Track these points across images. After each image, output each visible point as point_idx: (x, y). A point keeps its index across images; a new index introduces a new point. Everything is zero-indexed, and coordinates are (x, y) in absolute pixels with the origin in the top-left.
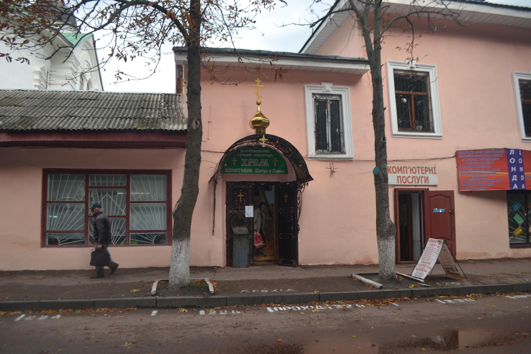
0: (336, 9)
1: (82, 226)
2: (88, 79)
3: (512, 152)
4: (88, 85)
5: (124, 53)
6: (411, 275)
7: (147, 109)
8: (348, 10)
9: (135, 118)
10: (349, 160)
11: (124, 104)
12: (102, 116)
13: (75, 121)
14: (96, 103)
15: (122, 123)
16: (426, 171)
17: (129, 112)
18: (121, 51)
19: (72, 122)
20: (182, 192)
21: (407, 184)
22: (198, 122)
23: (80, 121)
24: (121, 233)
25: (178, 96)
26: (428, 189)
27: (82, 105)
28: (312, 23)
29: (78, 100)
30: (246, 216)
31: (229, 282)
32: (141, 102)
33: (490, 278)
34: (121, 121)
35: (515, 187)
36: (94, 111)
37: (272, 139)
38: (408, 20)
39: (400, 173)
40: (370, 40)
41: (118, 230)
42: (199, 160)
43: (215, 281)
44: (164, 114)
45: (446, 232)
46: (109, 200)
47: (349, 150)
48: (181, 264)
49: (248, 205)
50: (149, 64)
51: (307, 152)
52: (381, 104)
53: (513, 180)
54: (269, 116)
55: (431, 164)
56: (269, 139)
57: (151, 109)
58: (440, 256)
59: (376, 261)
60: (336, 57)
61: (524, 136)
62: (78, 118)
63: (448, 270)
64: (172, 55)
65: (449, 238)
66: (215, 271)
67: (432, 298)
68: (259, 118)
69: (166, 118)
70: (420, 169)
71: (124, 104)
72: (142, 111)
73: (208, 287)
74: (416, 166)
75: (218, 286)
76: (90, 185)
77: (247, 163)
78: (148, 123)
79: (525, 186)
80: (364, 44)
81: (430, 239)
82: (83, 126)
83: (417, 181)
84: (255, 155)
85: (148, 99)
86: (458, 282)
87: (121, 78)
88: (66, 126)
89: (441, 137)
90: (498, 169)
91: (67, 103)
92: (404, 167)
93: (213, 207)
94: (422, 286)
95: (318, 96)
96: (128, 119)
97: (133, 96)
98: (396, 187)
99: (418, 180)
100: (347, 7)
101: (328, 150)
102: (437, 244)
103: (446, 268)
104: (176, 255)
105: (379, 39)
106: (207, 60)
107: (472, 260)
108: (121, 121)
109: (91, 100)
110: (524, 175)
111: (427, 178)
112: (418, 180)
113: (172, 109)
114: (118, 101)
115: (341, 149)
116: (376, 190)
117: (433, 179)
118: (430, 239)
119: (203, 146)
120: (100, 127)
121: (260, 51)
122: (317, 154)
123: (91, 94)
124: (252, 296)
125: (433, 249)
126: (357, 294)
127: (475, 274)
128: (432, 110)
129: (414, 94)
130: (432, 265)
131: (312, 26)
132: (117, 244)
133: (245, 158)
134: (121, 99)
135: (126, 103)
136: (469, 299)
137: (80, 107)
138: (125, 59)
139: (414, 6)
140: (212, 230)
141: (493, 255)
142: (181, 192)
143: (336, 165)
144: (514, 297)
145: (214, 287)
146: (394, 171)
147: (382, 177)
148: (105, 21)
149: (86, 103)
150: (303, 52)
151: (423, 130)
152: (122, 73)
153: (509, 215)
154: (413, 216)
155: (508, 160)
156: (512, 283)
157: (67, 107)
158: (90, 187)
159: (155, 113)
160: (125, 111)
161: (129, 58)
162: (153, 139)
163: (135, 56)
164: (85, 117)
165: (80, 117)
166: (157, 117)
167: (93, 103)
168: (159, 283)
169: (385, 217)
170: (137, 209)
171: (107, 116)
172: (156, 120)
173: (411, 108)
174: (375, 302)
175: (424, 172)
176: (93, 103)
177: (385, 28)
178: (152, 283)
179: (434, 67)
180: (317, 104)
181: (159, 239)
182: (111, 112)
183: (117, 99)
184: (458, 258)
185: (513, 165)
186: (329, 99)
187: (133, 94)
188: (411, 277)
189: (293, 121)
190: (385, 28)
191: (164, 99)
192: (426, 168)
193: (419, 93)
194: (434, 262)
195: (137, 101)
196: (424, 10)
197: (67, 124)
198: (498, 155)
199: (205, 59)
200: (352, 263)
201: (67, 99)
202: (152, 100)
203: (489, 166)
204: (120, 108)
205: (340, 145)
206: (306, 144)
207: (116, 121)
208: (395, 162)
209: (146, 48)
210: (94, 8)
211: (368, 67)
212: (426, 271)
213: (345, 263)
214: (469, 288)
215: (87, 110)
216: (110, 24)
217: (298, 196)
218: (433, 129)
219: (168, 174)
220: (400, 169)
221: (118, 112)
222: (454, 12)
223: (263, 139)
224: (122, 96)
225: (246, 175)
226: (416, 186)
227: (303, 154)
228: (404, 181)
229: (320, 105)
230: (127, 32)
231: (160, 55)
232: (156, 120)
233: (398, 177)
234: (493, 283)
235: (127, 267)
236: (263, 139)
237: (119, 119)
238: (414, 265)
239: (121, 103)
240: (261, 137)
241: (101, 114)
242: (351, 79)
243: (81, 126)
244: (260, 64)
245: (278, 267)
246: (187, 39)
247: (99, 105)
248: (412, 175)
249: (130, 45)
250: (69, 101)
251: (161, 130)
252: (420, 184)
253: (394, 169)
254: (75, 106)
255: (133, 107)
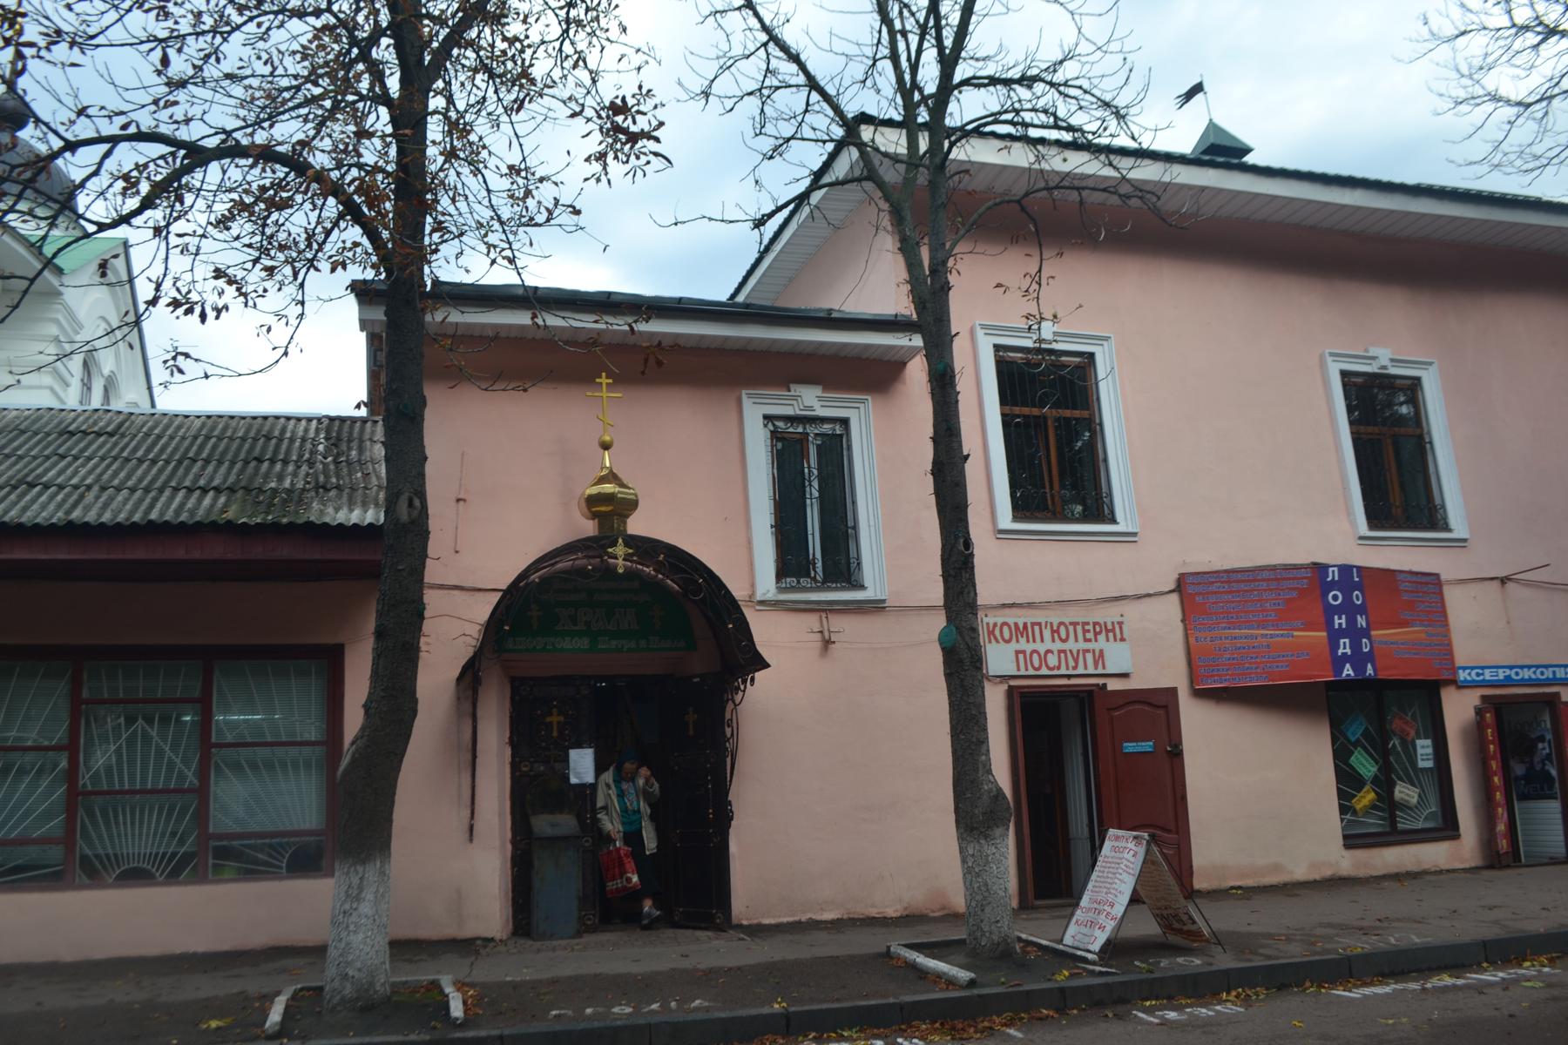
0: (826, 179)
1: (55, 825)
2: (106, 372)
3: (1333, 575)
4: (106, 389)
5: (194, 297)
6: (1060, 941)
7: (273, 461)
8: (859, 180)
9: (232, 490)
10: (875, 607)
11: (201, 447)
12: (130, 483)
13: (44, 498)
14: (115, 444)
15: (190, 505)
16: (1096, 634)
17: (215, 471)
18: (184, 291)
19: (33, 501)
20: (366, 713)
21: (1044, 671)
22: (417, 503)
23: (60, 497)
24: (182, 842)
25: (369, 424)
27: (70, 449)
28: (758, 216)
29: (61, 434)
30: (574, 780)
31: (515, 986)
32: (257, 440)
33: (1289, 939)
34: (187, 498)
35: (1348, 671)
36: (108, 467)
37: (646, 548)
38: (1023, 209)
39: (1023, 640)
40: (921, 264)
41: (173, 834)
42: (416, 614)
43: (472, 985)
44: (322, 478)
45: (1162, 813)
46: (147, 739)
47: (876, 579)
48: (361, 936)
49: (579, 746)
50: (269, 330)
51: (753, 585)
52: (955, 445)
53: (1340, 651)
54: (637, 483)
55: (1108, 615)
56: (637, 548)
57: (285, 462)
58: (1140, 878)
59: (959, 902)
60: (830, 311)
61: (1363, 527)
62: (53, 489)
63: (1169, 920)
64: (351, 305)
65: (1168, 827)
66: (477, 953)
67: (1120, 1009)
68: (608, 488)
69: (327, 490)
70: (1079, 628)
71: (201, 447)
72: (257, 469)
73: (447, 1003)
74: (1067, 621)
75: (479, 999)
76: (85, 694)
78: (271, 505)
79: (1375, 669)
80: (904, 275)
81: (1112, 832)
82: (68, 512)
83: (1071, 663)
85: (276, 433)
86: (1197, 956)
87: (181, 371)
88: (13, 513)
89: (1135, 534)
90: (1298, 623)
91: (25, 443)
92: (1033, 624)
93: (469, 756)
94: (1092, 973)
95: (780, 424)
96: (211, 493)
97: (233, 423)
98: (1013, 683)
99: (1076, 661)
100: (857, 173)
101: (814, 579)
102: (1131, 845)
103: (1162, 917)
104: (347, 907)
105: (944, 262)
106: (439, 317)
107: (1240, 888)
108: (187, 498)
109: (99, 434)
110: (1369, 638)
111: (1101, 652)
112: (1076, 661)
113: (349, 463)
114: (183, 438)
115: (850, 574)
116: (950, 694)
117: (1118, 657)
118: (1112, 832)
119: (432, 572)
120: (121, 517)
121: (610, 294)
122: (781, 590)
123: (100, 419)
124: (582, 1026)
125: (1120, 862)
126: (902, 1007)
127: (1245, 929)
128: (1106, 460)
129: (1053, 417)
130: (1119, 910)
131: (759, 223)
132: (119, 878)
134: (193, 432)
135: (209, 446)
136: (1229, 1005)
137: (63, 457)
138: (203, 317)
139: (1042, 171)
140: (466, 827)
141: (1300, 872)
142: (362, 712)
143: (838, 623)
144: (1356, 994)
145: (465, 1003)
146: (1007, 636)
147: (965, 655)
148: (133, 203)
149: (82, 445)
150: (740, 298)
151: (1086, 518)
152: (187, 355)
153: (1334, 752)
154: (1072, 763)
155: (1325, 595)
156: (1348, 952)
157: (21, 458)
158: (87, 702)
159: (295, 475)
160: (203, 468)
161: (211, 314)
162: (286, 551)
163: (226, 307)
164: (76, 487)
165: (61, 487)
166: (300, 485)
167: (104, 443)
168: (294, 997)
169: (976, 771)
170: (237, 767)
171: (145, 483)
172: (295, 496)
173: (1048, 456)
174: (953, 1028)
175: (1090, 635)
176: (104, 443)
177: (962, 232)
178: (268, 999)
179: (1107, 339)
180: (780, 445)
181: (305, 859)
182: (161, 471)
183: (181, 433)
184: (1199, 883)
185: (1339, 610)
186: (812, 430)
187: (232, 417)
188: (1061, 947)
189: (706, 493)
190: (962, 232)
191: (328, 431)
192: (1095, 624)
193: (1067, 413)
194: (1124, 899)
195: (243, 439)
196: (1065, 183)
197: (19, 507)
198: (1295, 584)
199: (437, 317)
200: (892, 912)
201: (23, 432)
202: (288, 435)
203: (1272, 616)
204: (186, 460)
205: (849, 564)
206: (746, 561)
207: (172, 498)
208: (1007, 611)
209: (268, 285)
210: (100, 164)
211: (917, 341)
212: (1102, 928)
213: (873, 912)
214: (1227, 972)
215: (83, 465)
216: (148, 213)
217: (728, 716)
218: (1112, 512)
219: (332, 660)
220: (1022, 631)
221: (181, 471)
222: (1147, 188)
223: (620, 550)
224: (198, 423)
225: (567, 651)
226: (1069, 677)
227: (738, 591)
228: (1037, 664)
229: (788, 447)
230: (203, 236)
231: (302, 303)
232: (295, 496)
233: (1017, 652)
234: (1295, 953)
235: (201, 949)
236: (620, 550)
237: (181, 494)
238: (1069, 910)
239: (192, 444)
240: (614, 544)
241: (128, 477)
242: (876, 375)
243: (60, 514)
244: (599, 332)
245: (670, 932)
246: (385, 258)
247: (123, 450)
248: (1059, 645)
249: (219, 274)
250: (30, 438)
251: (309, 525)
252: (1080, 671)
253: (1006, 629)
254: (46, 453)
255: (229, 457)
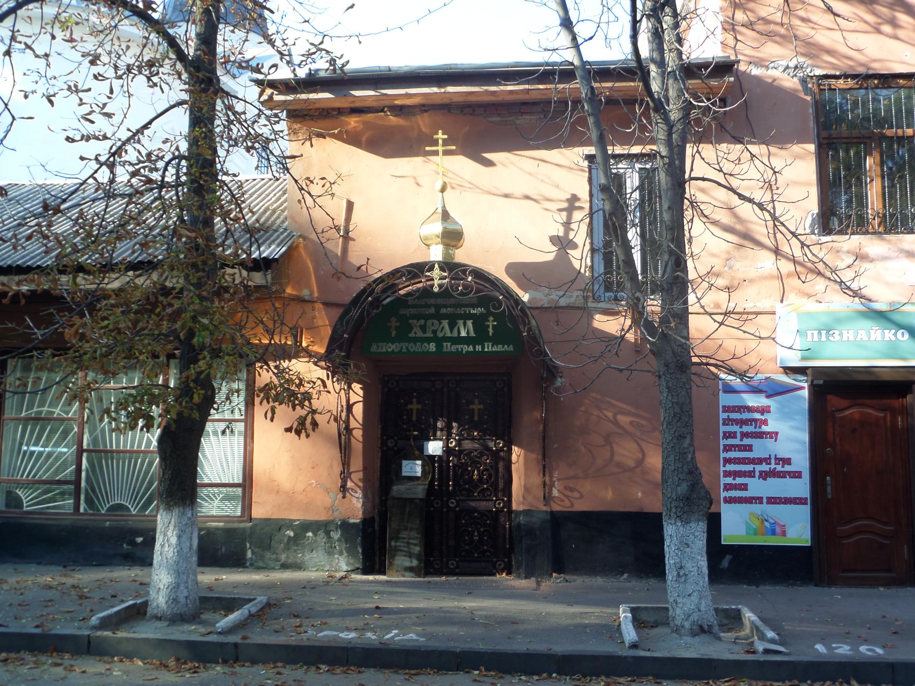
3: (825, 134)
26: (734, 479)
77: (423, 328)
84: (443, 311)
133: (418, 317)
